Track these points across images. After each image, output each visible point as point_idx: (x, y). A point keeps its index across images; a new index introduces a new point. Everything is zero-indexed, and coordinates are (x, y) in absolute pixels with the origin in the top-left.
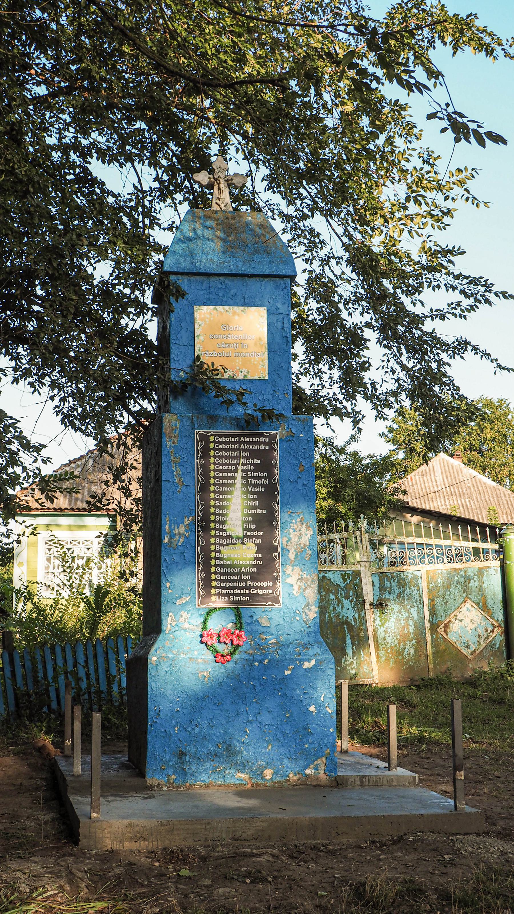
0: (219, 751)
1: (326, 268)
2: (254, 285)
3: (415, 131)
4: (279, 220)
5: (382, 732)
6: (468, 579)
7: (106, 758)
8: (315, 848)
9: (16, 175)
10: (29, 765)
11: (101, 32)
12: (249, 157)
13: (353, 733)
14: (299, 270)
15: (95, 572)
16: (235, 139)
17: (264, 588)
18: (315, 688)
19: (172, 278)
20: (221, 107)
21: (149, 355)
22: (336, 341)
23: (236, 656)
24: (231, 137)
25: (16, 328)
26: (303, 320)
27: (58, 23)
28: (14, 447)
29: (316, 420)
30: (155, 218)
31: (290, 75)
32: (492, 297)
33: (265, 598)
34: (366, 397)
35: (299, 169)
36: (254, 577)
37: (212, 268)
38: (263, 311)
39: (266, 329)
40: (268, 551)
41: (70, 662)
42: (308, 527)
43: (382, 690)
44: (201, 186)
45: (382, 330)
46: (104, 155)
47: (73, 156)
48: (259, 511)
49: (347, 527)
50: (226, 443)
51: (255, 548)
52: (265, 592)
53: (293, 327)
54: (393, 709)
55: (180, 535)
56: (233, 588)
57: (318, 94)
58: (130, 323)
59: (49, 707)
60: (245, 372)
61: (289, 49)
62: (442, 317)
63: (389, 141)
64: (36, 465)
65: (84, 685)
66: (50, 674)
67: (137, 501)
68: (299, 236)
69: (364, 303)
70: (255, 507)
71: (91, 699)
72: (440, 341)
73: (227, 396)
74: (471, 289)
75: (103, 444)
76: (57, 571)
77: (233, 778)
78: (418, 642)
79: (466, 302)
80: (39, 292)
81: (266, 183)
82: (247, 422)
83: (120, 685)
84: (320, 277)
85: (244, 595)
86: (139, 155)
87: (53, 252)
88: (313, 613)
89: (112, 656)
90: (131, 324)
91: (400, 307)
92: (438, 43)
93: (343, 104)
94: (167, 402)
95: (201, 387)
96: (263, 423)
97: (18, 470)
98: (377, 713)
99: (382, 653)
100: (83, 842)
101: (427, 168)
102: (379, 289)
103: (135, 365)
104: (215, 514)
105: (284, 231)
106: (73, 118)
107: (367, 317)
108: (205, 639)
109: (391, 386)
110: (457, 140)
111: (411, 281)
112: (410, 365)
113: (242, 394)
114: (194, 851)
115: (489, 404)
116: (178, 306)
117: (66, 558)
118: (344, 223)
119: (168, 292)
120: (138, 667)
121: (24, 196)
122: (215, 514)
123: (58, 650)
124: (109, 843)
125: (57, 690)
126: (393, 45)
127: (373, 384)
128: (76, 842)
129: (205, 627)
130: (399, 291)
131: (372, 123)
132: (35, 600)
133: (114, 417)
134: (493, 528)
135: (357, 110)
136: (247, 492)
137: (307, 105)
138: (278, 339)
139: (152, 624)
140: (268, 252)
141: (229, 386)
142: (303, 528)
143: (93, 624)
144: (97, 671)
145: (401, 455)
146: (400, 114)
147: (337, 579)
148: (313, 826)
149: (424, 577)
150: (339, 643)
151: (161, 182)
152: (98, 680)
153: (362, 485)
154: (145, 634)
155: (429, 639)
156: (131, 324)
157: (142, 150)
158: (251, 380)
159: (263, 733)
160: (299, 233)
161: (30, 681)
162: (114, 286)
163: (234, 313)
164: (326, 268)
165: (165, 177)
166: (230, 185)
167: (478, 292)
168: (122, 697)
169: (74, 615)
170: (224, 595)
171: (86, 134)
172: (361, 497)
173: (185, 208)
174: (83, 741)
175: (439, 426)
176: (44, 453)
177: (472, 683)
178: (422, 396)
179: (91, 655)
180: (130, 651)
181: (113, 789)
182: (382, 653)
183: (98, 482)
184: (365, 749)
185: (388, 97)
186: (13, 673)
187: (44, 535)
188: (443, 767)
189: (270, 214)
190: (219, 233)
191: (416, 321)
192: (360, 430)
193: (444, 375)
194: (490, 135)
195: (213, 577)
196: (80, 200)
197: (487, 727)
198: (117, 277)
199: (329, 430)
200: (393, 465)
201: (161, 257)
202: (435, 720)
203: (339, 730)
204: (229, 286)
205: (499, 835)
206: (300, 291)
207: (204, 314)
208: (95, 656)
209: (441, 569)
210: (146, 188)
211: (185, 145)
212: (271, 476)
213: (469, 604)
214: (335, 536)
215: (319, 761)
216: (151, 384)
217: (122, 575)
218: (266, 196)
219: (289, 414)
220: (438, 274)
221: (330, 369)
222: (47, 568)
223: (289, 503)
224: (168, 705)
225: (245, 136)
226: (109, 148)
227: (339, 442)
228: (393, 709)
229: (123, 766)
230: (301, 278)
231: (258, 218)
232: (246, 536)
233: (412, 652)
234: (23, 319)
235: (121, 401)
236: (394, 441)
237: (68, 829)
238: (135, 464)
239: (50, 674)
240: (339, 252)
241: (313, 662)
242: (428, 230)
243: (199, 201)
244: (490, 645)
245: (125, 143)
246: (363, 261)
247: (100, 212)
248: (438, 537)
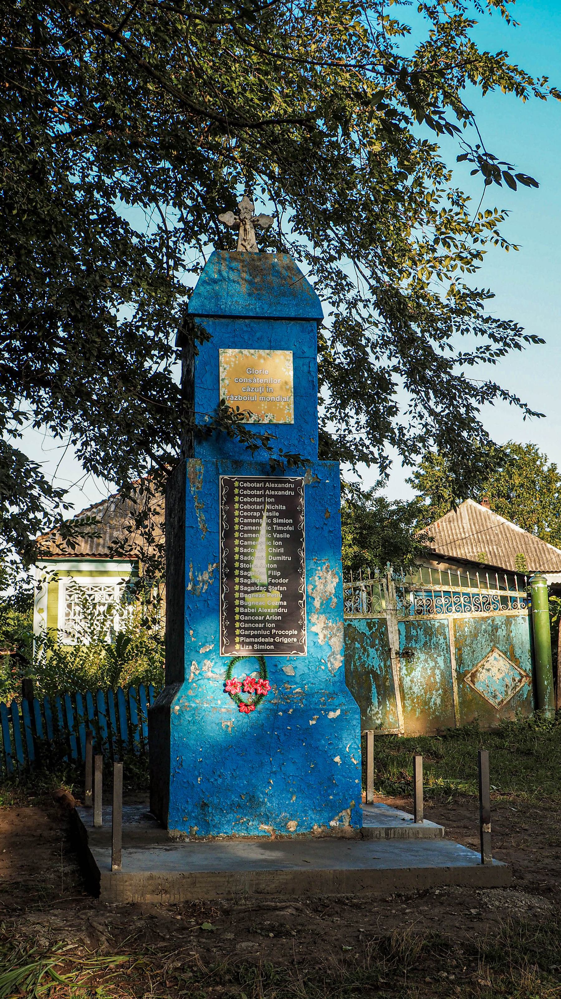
2: (281, 328)
3: (445, 171)
4: (305, 262)
5: (408, 784)
6: (495, 628)
8: (340, 902)
9: (38, 215)
10: (49, 816)
11: (126, 69)
12: (275, 197)
13: (379, 784)
15: (117, 618)
16: (261, 179)
17: (289, 637)
19: (197, 320)
21: (173, 399)
22: (363, 385)
23: (260, 706)
25: (37, 371)
26: (330, 363)
27: (81, 60)
28: (35, 492)
29: (342, 466)
30: (179, 259)
31: (318, 114)
32: (521, 341)
33: (290, 647)
34: (393, 442)
35: (326, 210)
36: (280, 625)
37: (238, 310)
38: (289, 354)
39: (291, 373)
40: (293, 599)
41: (91, 711)
42: (334, 575)
43: (408, 740)
44: (226, 226)
45: (410, 374)
46: (128, 195)
48: (284, 558)
49: (373, 574)
50: (251, 489)
51: (279, 596)
52: (289, 640)
53: (320, 371)
54: (419, 760)
55: (204, 582)
57: (346, 134)
58: (154, 366)
60: (270, 416)
61: (316, 87)
62: (471, 361)
63: (418, 182)
64: (57, 510)
66: (71, 723)
68: (326, 278)
69: (392, 347)
70: (280, 554)
71: (113, 748)
73: (252, 441)
75: (126, 488)
76: (77, 618)
78: (445, 691)
79: (496, 347)
80: (62, 334)
82: (273, 467)
83: (141, 734)
85: (269, 644)
86: (163, 195)
87: (77, 293)
88: (338, 662)
89: (133, 705)
90: (155, 367)
92: (468, 82)
93: (371, 144)
94: (191, 447)
95: (225, 433)
96: (290, 466)
97: (40, 515)
98: (402, 764)
99: (408, 703)
100: (104, 894)
101: (456, 209)
103: (158, 408)
104: (239, 561)
105: (311, 273)
106: (97, 157)
107: (395, 361)
108: (228, 688)
109: (419, 431)
110: (488, 182)
111: (439, 325)
112: (438, 410)
113: (268, 439)
114: (216, 904)
115: (517, 449)
116: (202, 349)
117: (87, 604)
118: (371, 265)
119: (194, 336)
120: (161, 716)
123: (79, 698)
124: (130, 896)
125: (78, 739)
126: (419, 87)
127: (401, 429)
129: (228, 675)
130: (427, 334)
131: (401, 164)
132: (56, 647)
134: (521, 576)
135: (385, 150)
136: (272, 539)
137: (335, 145)
139: (175, 672)
141: (254, 431)
142: (329, 576)
143: (115, 672)
144: (118, 719)
145: (428, 501)
146: (429, 154)
147: (362, 627)
148: (339, 879)
149: (451, 625)
150: (364, 692)
151: (186, 223)
152: (119, 729)
153: (389, 532)
154: (167, 683)
155: (456, 689)
156: (155, 367)
157: (166, 190)
158: (276, 425)
160: (326, 275)
161: (50, 729)
162: (138, 328)
163: (260, 357)
164: (354, 311)
165: (190, 218)
166: (256, 225)
167: (507, 336)
168: (143, 746)
169: (96, 663)
171: (110, 174)
172: (387, 543)
173: (209, 249)
174: (104, 792)
175: (468, 472)
176: (66, 498)
177: (499, 733)
178: (450, 441)
179: (112, 703)
180: (153, 700)
181: (134, 841)
182: (408, 703)
183: (120, 528)
184: (391, 800)
185: (417, 137)
186: (33, 722)
187: (65, 581)
189: (296, 255)
190: (244, 275)
191: (444, 365)
193: (473, 420)
196: (104, 241)
197: (514, 779)
199: (358, 475)
200: (420, 511)
201: (186, 298)
203: (364, 781)
204: (258, 330)
207: (229, 357)
208: (117, 705)
209: (469, 617)
210: (170, 228)
211: (210, 185)
212: (296, 523)
214: (361, 584)
215: (344, 813)
216: (175, 428)
217: (145, 623)
218: (293, 237)
219: (315, 459)
220: (466, 318)
221: (357, 413)
222: (68, 615)
223: (315, 551)
225: (271, 176)
226: (133, 188)
227: (365, 488)
228: (419, 760)
229: (145, 817)
230: (328, 321)
231: (285, 260)
232: (270, 584)
233: (438, 701)
235: (145, 445)
236: (420, 487)
238: (158, 509)
239: (71, 723)
240: (367, 294)
241: (338, 712)
242: (457, 272)
243: (224, 242)
244: (518, 695)
245: (149, 182)
246: (391, 304)
247: (124, 253)
248: (465, 585)
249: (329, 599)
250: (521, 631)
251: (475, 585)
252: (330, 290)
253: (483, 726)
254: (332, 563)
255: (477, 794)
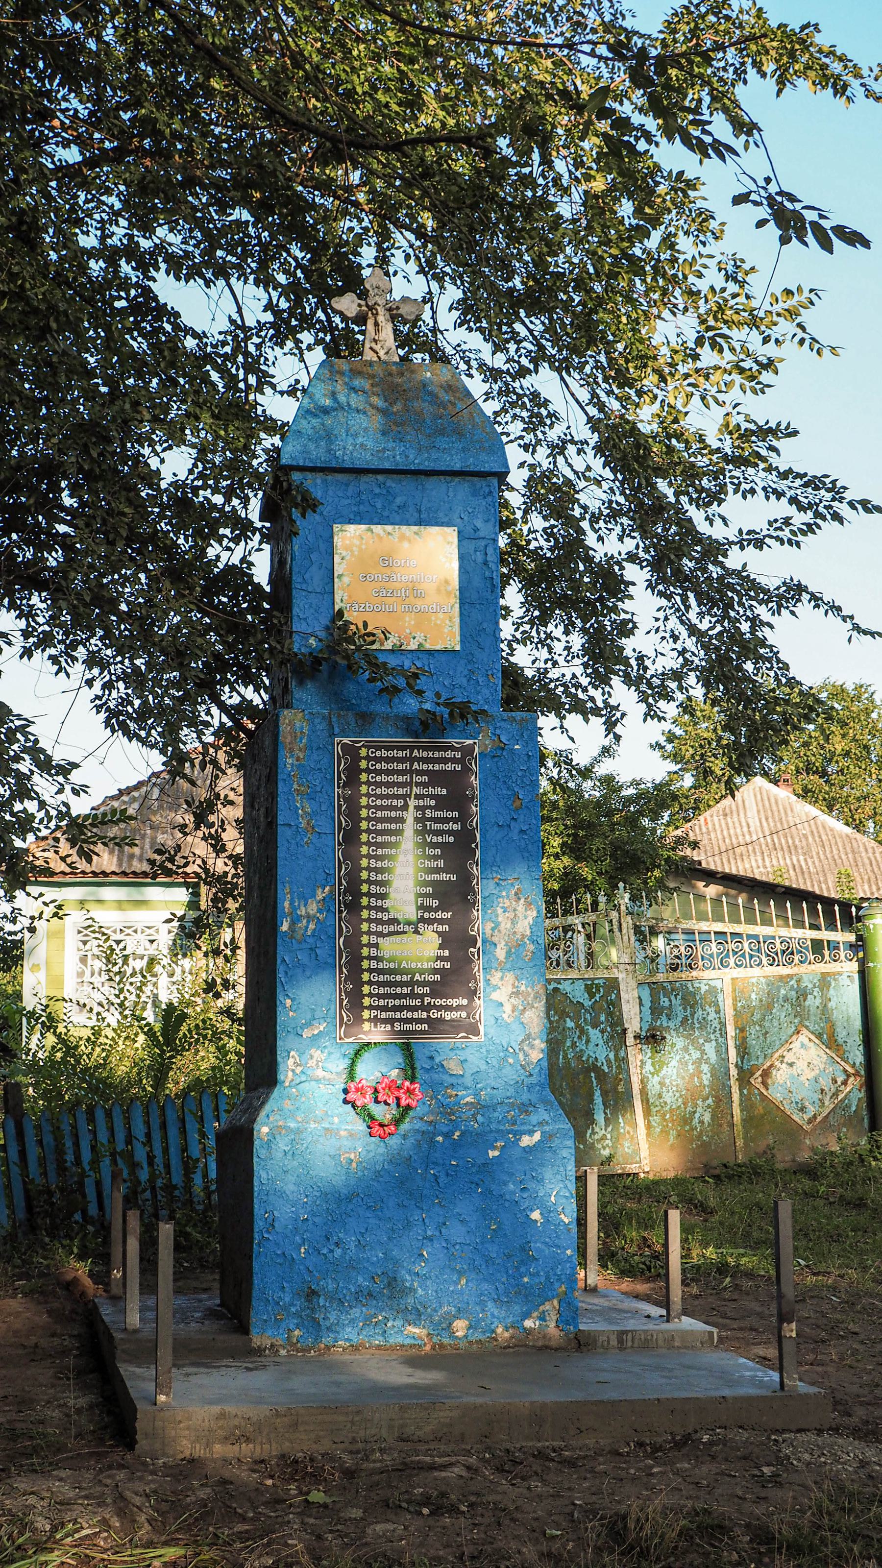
0: (376, 1288)
1: (560, 460)
2: (436, 488)
3: (713, 224)
4: (478, 377)
5: (656, 1257)
6: (803, 994)
7: (182, 1301)
8: (541, 1455)
9: (27, 301)
10: (50, 1312)
12: (427, 269)
13: (606, 1257)
14: (513, 464)
15: (164, 981)
16: (402, 239)
17: (453, 1009)
18: (540, 1181)
19: (296, 476)
20: (379, 184)
21: (255, 610)
22: (576, 585)
23: (405, 1126)
24: (397, 235)
25: (27, 563)
26: (520, 548)
27: (99, 39)
28: (25, 766)
29: (542, 721)
30: (266, 374)
31: (498, 128)
32: (843, 509)
33: (455, 1027)
34: (628, 680)
35: (512, 290)
36: (437, 990)
37: (364, 459)
38: (451, 534)
39: (456, 565)
40: (460, 946)
41: (120, 1136)
42: (528, 905)
43: (656, 1183)
44: (344, 318)
45: (656, 565)
46: (178, 266)
47: (126, 268)
48: (445, 877)
49: (595, 904)
50: (388, 760)
51: (437, 941)
52: (454, 1015)
53: (503, 562)
54: (674, 1216)
55: (309, 917)
56: (400, 1008)
57: (546, 161)
58: (223, 554)
59: (84, 1212)
60: (420, 637)
61: (495, 83)
62: (759, 544)
63: (668, 242)
64: (61, 797)
65: (144, 1175)
66: (86, 1156)
67: (235, 859)
68: (513, 405)
69: (625, 521)
70: (437, 870)
71: (156, 1200)
72: (755, 586)
74: (808, 496)
75: (177, 761)
76: (97, 980)
77: (400, 1335)
78: (718, 1101)
79: (800, 519)
80: (68, 501)
81: (456, 314)
82: (425, 724)
83: (205, 1175)
84: (548, 475)
85: (419, 1021)
86: (238, 267)
87: (90, 433)
88: (537, 1052)
89: (192, 1126)
90: (225, 556)
91: (687, 527)
92: (752, 74)
93: (588, 178)
94: (286, 690)
95: (345, 665)
96: (452, 725)
97: (31, 806)
98: (646, 1224)
99: (655, 1120)
100: (143, 1443)
101: (732, 288)
102: (650, 495)
103: (230, 625)
104: (369, 882)
105: (488, 396)
106: (125, 202)
107: (629, 545)
108: (351, 1096)
109: (671, 662)
110: (784, 240)
111: (705, 482)
112: (704, 626)
113: (416, 676)
114: (332, 1459)
115: (839, 692)
116: (306, 525)
117: (113, 957)
118: (590, 382)
119: (289, 502)
120: (237, 1145)
121: (42, 337)
122: (369, 882)
123: (100, 1115)
124: (187, 1447)
125: (98, 1184)
126: (675, 78)
127: (640, 659)
128: (131, 1445)
129: (351, 1076)
130: (684, 499)
131: (638, 211)
132: (61, 1029)
133: (195, 715)
134: (845, 906)
135: (612, 188)
136: (424, 844)
137: (527, 181)
138: (477, 581)
139: (261, 1070)
140: (459, 433)
141: (393, 662)
142: (521, 907)
143: (160, 1071)
144: (166, 1150)
145: (688, 780)
147: (578, 993)
148: (538, 1417)
149: (728, 990)
151: (277, 313)
152: (167, 1166)
153: (621, 833)
154: (249, 1088)
155: (736, 1097)
156: (225, 556)
157: (243, 257)
158: (430, 652)
159: (451, 1257)
160: (513, 400)
161: (51, 1167)
162: (195, 490)
163: (402, 538)
164: (560, 460)
165: (284, 304)
166: (395, 316)
167: (820, 500)
168: (209, 1195)
169: (128, 1055)
170: (385, 1021)
171: (148, 230)
172: (619, 852)
173: (317, 356)
174: (143, 1272)
175: (754, 730)
176: (76, 777)
177: (810, 1171)
178: (725, 679)
180: (224, 1116)
181: (193, 1354)
182: (655, 1120)
183: (168, 826)
184: (626, 1285)
186: (23, 1154)
187: (75, 918)
188: (761, 1316)
189: (463, 366)
190: (375, 400)
191: (714, 550)
192: (618, 738)
193: (763, 643)
194: (841, 231)
195: (366, 989)
196: (138, 344)
197: (835, 1248)
198: (201, 476)
199: (565, 737)
200: (674, 797)
201: (277, 440)
202: (747, 1235)
203: (582, 1251)
204: (393, 492)
205: (857, 1433)
206: (515, 500)
207: (350, 538)
208: (164, 1126)
209: (757, 976)
210: (250, 322)
211: (317, 249)
212: (464, 817)
213: (804, 1037)
214: (575, 920)
215: (547, 1306)
216: (260, 658)
217: (210, 987)
218: (456, 336)
219: (496, 710)
220: (751, 471)
221: (567, 633)
222: (81, 974)
224: (288, 1209)
225: (420, 233)
226: (187, 255)
227: (581, 759)
228: (674, 1216)
229: (212, 1314)
231: (443, 373)
232: (422, 920)
233: (707, 1118)
234: (40, 547)
235: (208, 687)
236: (676, 757)
237: (117, 1423)
238: (232, 796)
239: (86, 1156)
240: (582, 432)
241: (537, 1136)
242: (735, 394)
243: (341, 345)
244: (841, 1107)
245: (214, 245)
246: (622, 447)
247: (172, 364)
248: (751, 921)
249: (520, 945)
250: (846, 1000)
251: (767, 922)
252: (521, 426)
253: (783, 1159)
254: (526, 885)
255: (773, 1272)
